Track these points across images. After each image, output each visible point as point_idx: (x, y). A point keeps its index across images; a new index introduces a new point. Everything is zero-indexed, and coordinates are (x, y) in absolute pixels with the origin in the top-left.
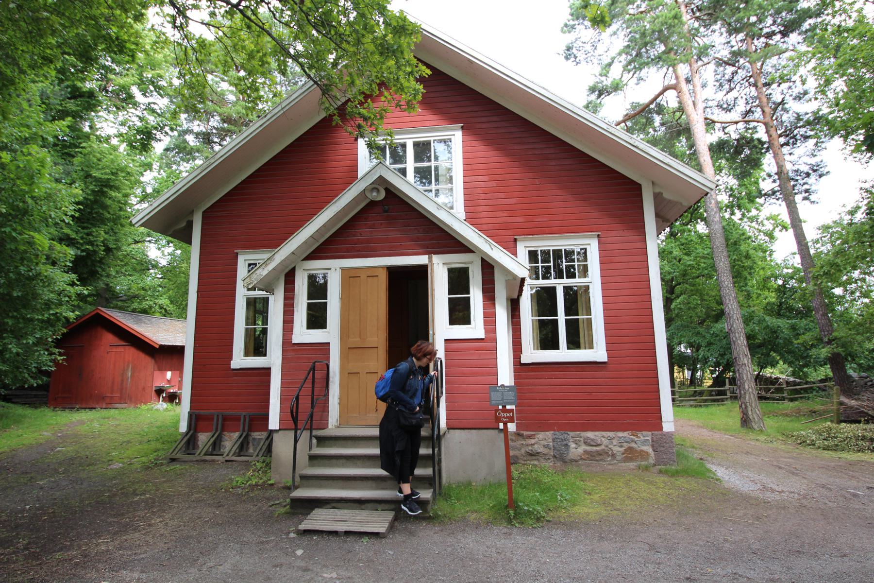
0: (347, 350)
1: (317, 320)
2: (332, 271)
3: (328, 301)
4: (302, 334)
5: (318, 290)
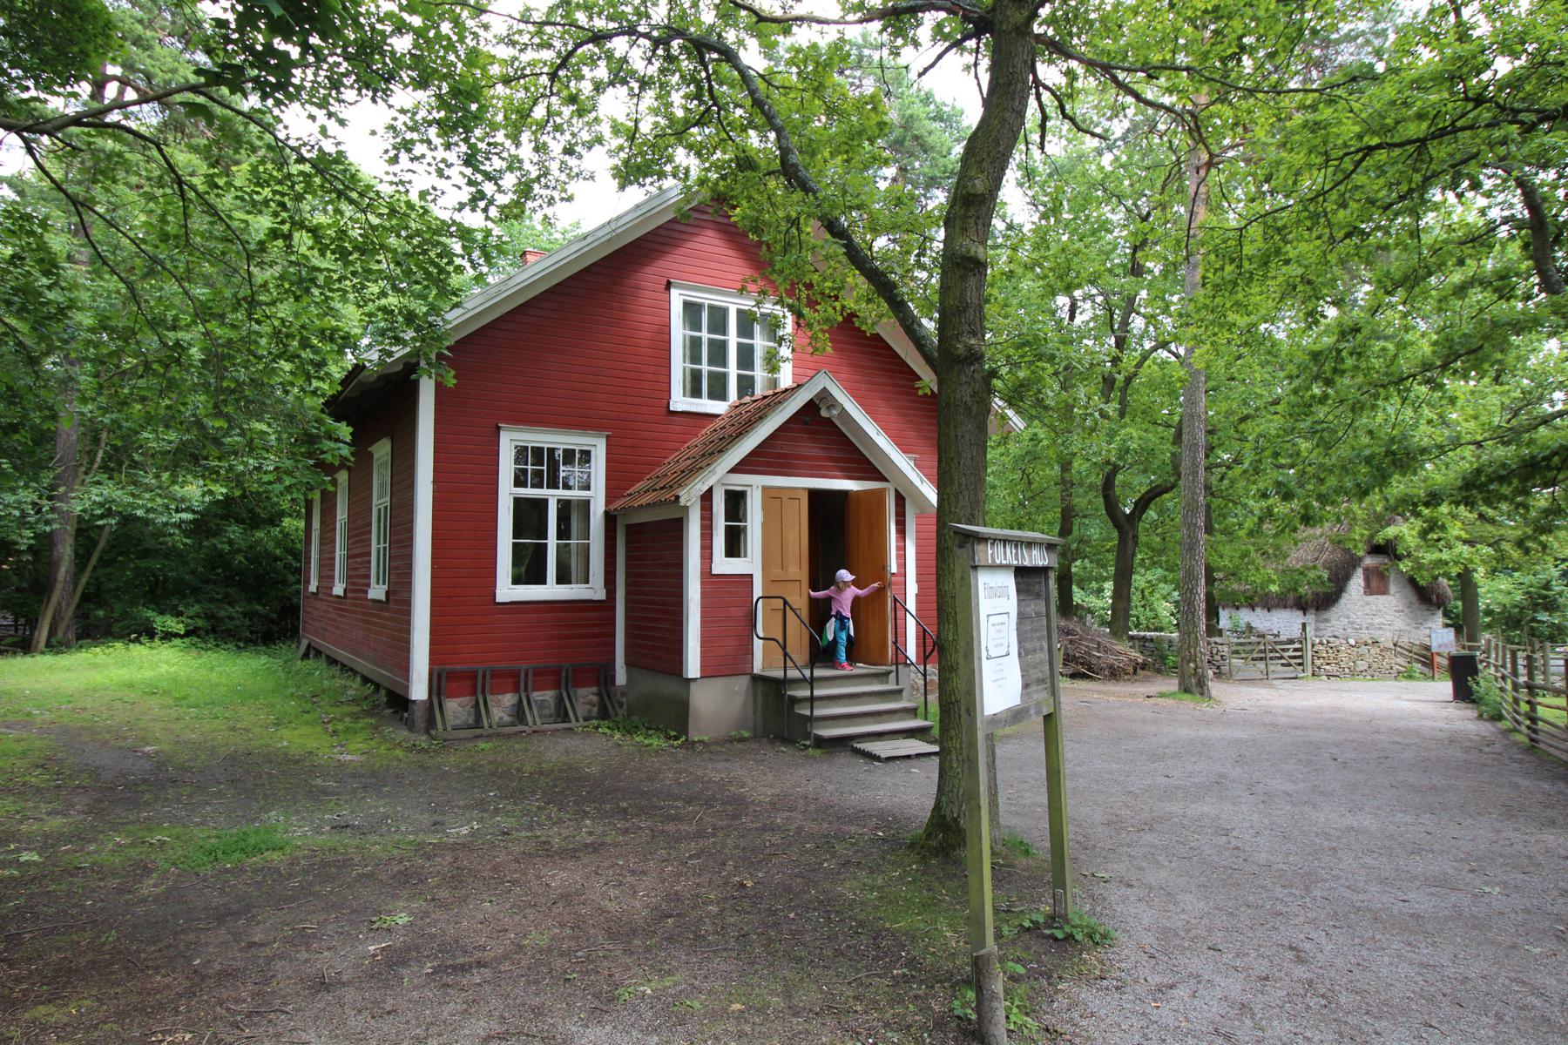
0: (768, 581)
1: (734, 546)
2: (755, 485)
3: (749, 524)
4: (723, 565)
5: (736, 501)
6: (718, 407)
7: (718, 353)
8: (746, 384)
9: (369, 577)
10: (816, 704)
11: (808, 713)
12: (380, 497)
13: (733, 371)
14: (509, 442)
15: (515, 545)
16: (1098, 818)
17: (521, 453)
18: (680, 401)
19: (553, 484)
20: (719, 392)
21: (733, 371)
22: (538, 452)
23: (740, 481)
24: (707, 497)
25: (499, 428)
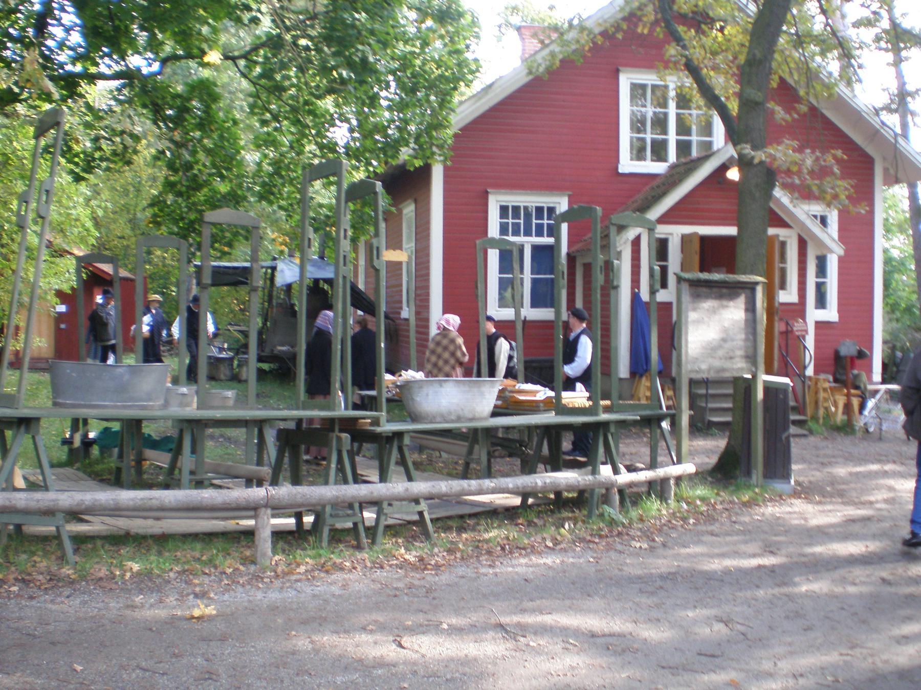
2: (675, 232)
6: (659, 168)
7: (660, 123)
8: (683, 148)
9: (401, 302)
10: (710, 399)
11: (703, 405)
12: (408, 243)
13: (672, 137)
14: (625, 81)
15: (500, 278)
16: (67, 128)
17: (504, 210)
18: (627, 164)
19: (528, 233)
20: (659, 151)
21: (672, 137)
22: (516, 209)
23: (662, 230)
24: (636, 242)
25: (487, 193)
